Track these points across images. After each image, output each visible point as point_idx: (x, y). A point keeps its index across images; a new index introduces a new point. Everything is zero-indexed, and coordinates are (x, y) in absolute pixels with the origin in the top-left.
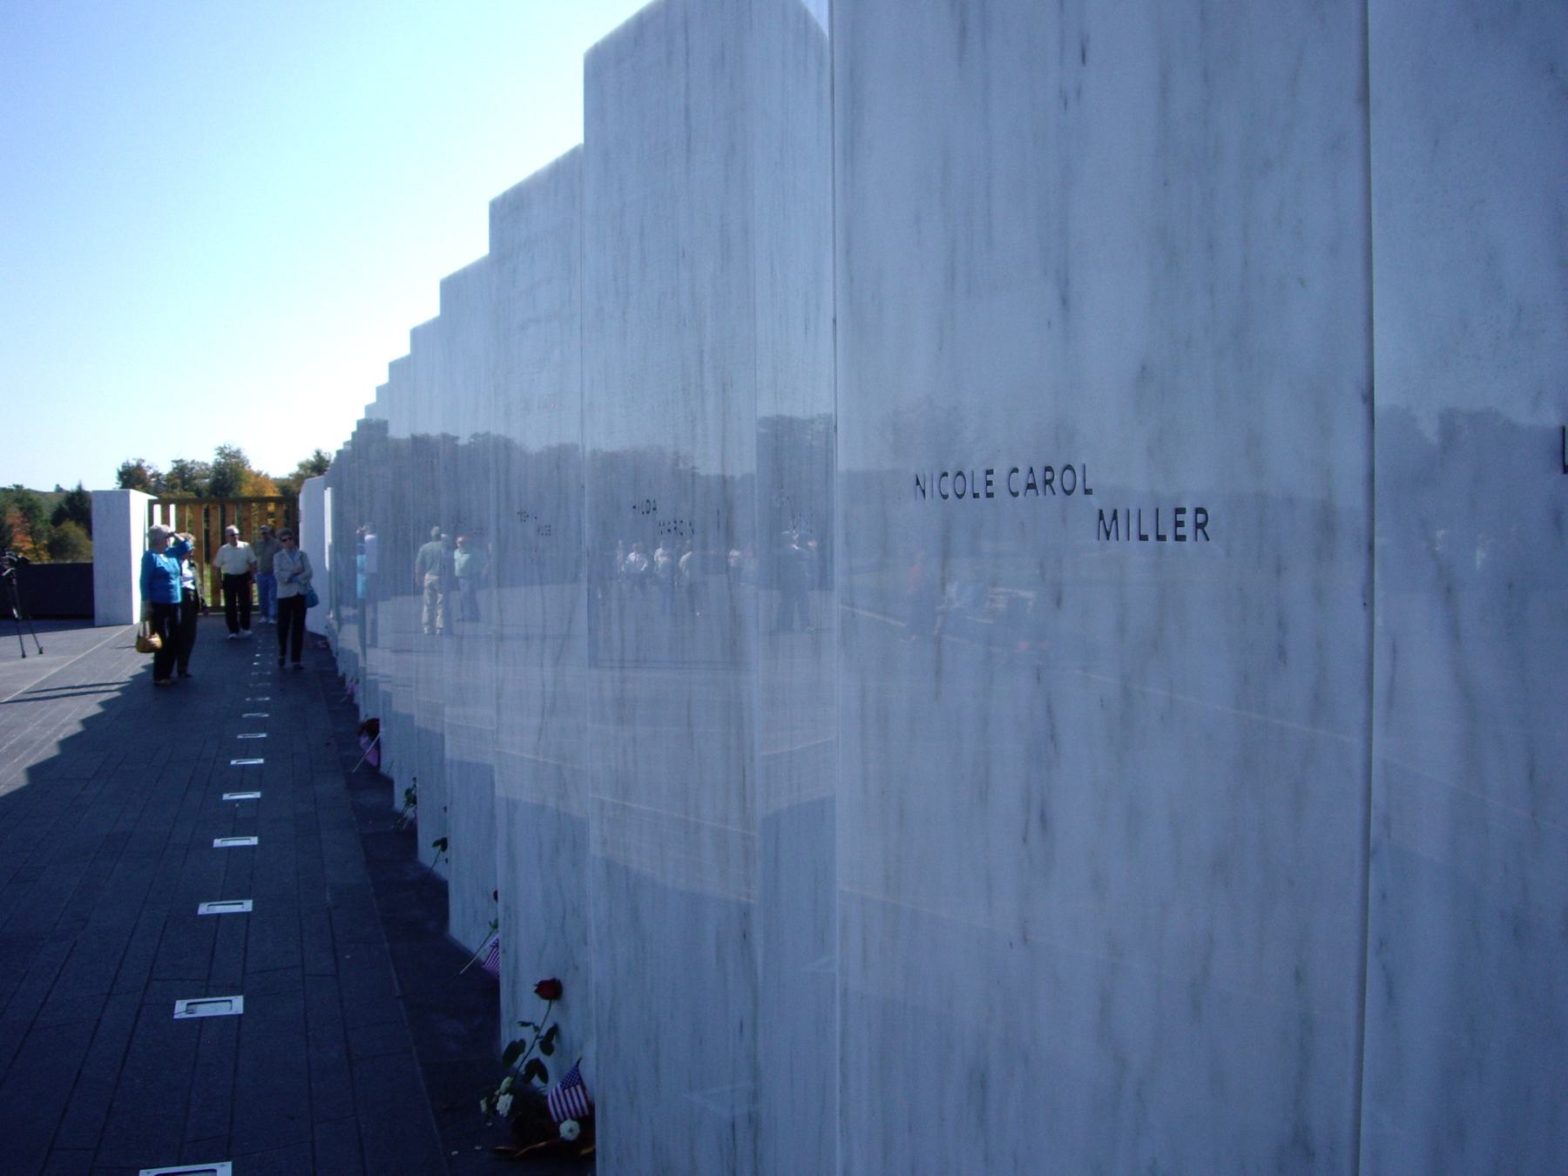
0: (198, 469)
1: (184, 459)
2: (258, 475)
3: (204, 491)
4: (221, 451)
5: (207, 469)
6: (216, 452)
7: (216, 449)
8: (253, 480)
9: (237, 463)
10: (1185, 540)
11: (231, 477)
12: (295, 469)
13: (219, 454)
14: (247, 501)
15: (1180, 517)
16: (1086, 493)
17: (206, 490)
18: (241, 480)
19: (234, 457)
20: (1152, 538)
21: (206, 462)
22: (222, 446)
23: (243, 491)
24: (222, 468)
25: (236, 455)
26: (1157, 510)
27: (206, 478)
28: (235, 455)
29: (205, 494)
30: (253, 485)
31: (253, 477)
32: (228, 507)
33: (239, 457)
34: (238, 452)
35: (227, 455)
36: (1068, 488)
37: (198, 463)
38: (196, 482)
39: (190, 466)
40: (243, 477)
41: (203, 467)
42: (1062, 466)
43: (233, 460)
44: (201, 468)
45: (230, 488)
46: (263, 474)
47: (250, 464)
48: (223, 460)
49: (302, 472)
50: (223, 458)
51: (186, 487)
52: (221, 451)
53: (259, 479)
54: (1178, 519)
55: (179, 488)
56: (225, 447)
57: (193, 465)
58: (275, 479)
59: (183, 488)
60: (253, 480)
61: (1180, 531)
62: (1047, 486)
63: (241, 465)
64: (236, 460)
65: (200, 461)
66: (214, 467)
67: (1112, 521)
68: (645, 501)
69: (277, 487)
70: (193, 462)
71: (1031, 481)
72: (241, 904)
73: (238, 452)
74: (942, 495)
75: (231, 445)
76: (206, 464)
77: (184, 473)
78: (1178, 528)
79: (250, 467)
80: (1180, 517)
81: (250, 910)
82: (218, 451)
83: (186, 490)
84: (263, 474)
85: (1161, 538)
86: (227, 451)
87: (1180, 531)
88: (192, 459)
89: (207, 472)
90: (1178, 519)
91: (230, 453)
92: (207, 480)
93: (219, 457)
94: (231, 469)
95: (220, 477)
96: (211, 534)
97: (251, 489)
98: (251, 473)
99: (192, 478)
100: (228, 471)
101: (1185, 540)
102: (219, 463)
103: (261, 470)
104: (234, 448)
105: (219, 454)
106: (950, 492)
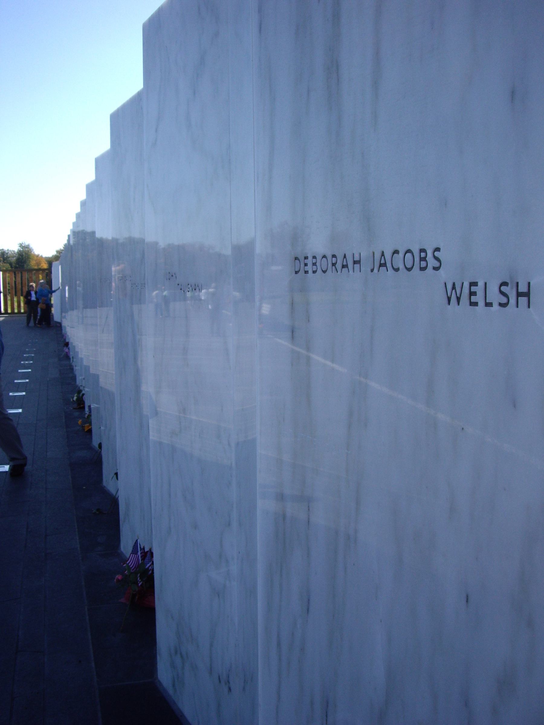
0: (10, 253)
1: (4, 249)
2: (38, 256)
3: (13, 264)
4: (21, 245)
5: (15, 253)
6: (18, 246)
7: (19, 244)
8: (35, 258)
9: (28, 251)
10: (477, 306)
11: (25, 257)
12: (54, 253)
13: (20, 246)
14: (30, 271)
15: (473, 289)
16: (305, 273)
17: (14, 263)
18: (30, 258)
19: (27, 248)
20: (481, 303)
21: (14, 250)
22: (21, 243)
23: (31, 263)
24: (22, 253)
25: (28, 247)
26: (445, 284)
27: (14, 257)
28: (28, 247)
29: (14, 265)
30: (36, 261)
31: (35, 257)
32: (23, 273)
33: (29, 248)
34: (29, 245)
35: (23, 247)
36: (409, 266)
37: (10, 250)
38: (10, 259)
39: (7, 252)
40: (30, 257)
41: (13, 252)
42: (406, 249)
43: (26, 249)
44: (12, 253)
45: (25, 262)
46: (40, 255)
47: (34, 251)
48: (22, 249)
49: (58, 254)
50: (22, 248)
51: (5, 261)
52: (21, 245)
53: (38, 258)
54: (472, 290)
55: (2, 262)
56: (23, 243)
57: (8, 252)
58: (46, 258)
59: (4, 262)
60: (35, 258)
61: (473, 299)
62: (333, 267)
63: (30, 251)
64: (28, 249)
65: (11, 250)
66: (18, 252)
67: (453, 290)
68: (168, 273)
69: (46, 261)
70: (8, 250)
71: (383, 262)
72: (4, 467)
73: (29, 245)
74: (323, 271)
75: (25, 242)
76: (14, 251)
77: (4, 255)
78: (472, 297)
79: (34, 252)
80: (473, 289)
81: (7, 470)
82: (19, 245)
83: (5, 263)
84: (40, 255)
85: (488, 305)
86: (23, 245)
87: (473, 299)
88: (8, 249)
89: (15, 255)
90: (472, 290)
91: (25, 246)
92: (15, 258)
93: (20, 248)
94: (25, 253)
95: (20, 257)
96: (17, 283)
97: (35, 262)
98: (35, 255)
99: (8, 257)
100: (24, 254)
101: (477, 306)
102: (20, 251)
103: (39, 253)
104: (27, 244)
105: (20, 246)
106: (401, 266)
